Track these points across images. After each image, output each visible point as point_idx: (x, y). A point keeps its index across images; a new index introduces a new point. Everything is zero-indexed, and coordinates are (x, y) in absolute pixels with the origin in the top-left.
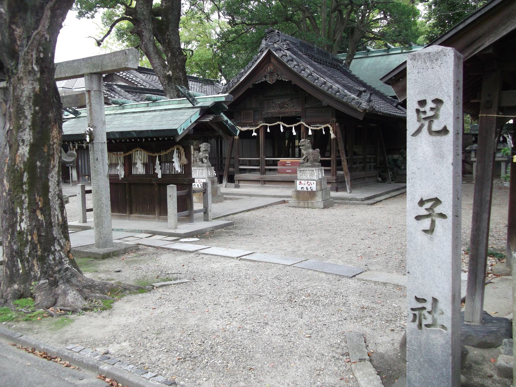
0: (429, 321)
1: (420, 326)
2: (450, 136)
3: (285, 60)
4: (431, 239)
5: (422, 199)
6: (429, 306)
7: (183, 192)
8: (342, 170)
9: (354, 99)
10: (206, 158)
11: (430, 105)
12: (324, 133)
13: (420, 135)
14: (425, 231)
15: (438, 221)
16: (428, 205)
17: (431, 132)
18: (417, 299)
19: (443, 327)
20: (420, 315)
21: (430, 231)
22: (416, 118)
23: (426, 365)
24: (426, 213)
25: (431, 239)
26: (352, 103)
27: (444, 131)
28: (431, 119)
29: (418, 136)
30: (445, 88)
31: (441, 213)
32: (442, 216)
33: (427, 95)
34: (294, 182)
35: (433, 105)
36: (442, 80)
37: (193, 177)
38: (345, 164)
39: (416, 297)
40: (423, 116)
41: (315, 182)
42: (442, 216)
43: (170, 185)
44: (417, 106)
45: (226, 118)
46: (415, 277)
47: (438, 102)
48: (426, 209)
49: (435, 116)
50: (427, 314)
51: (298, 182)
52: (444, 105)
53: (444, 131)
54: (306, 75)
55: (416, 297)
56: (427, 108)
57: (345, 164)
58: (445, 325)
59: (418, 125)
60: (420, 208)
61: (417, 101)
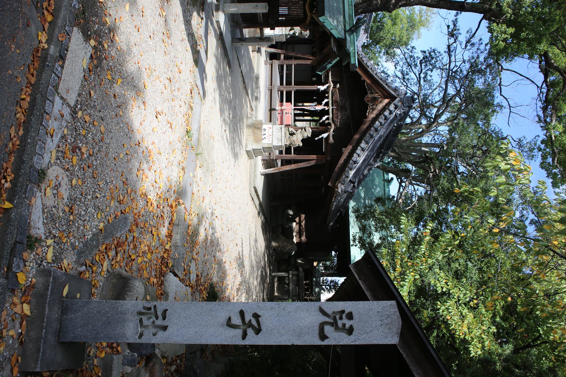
0: (145, 322)
1: (140, 313)
2: (319, 342)
3: (387, 113)
4: (222, 325)
5: (260, 316)
6: (159, 322)
7: (261, 19)
8: (282, 165)
9: (347, 177)
10: (294, 33)
11: (348, 323)
12: (316, 139)
13: (321, 314)
14: (230, 319)
15: (239, 332)
16: (254, 322)
17: (322, 326)
18: (166, 311)
19: (141, 336)
20: (150, 314)
21: (229, 324)
22: (336, 311)
23: (104, 319)
24: (247, 320)
25: (222, 325)
26: (344, 176)
27: (323, 337)
28: (334, 324)
29: (319, 312)
30: (363, 337)
31: (247, 335)
32: (244, 336)
33: (357, 320)
34: (270, 122)
35: (347, 326)
36: (370, 334)
37: (276, 28)
38: (287, 168)
39: (167, 310)
40: (338, 317)
41: (271, 142)
42: (244, 336)
43: (268, 6)
44: (347, 311)
45: (334, 62)
46: (185, 310)
47: (350, 331)
48: (250, 320)
49: (337, 328)
50: (151, 320)
51: (271, 126)
52: (347, 336)
53: (323, 337)
54: (371, 132)
55: (167, 310)
56: (345, 321)
57: (287, 168)
58: (143, 337)
59: (329, 312)
60: (251, 315)
61: (352, 311)
